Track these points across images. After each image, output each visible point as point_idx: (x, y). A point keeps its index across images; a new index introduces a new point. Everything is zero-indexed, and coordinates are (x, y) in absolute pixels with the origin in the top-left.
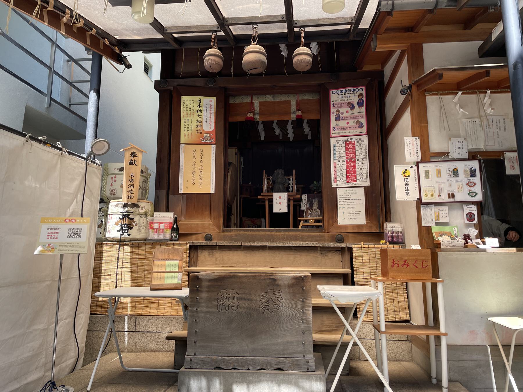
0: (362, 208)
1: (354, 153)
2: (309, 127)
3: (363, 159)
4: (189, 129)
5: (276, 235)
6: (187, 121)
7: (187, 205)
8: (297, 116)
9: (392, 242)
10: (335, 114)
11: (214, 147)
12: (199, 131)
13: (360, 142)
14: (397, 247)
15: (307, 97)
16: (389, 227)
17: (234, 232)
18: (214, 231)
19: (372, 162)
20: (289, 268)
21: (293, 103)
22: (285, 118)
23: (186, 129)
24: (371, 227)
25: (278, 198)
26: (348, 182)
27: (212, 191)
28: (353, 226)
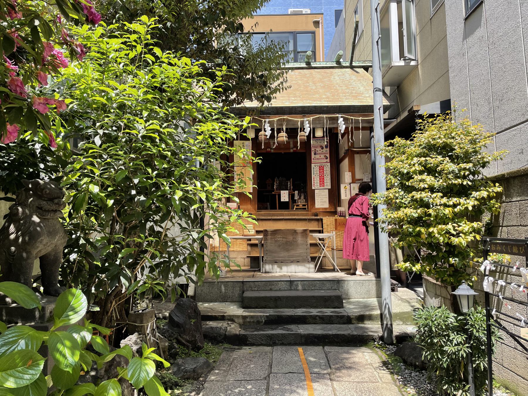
0: (327, 200)
9: (340, 216)
14: (342, 218)
16: (339, 209)
17: (263, 212)
20: (300, 227)
28: (323, 208)
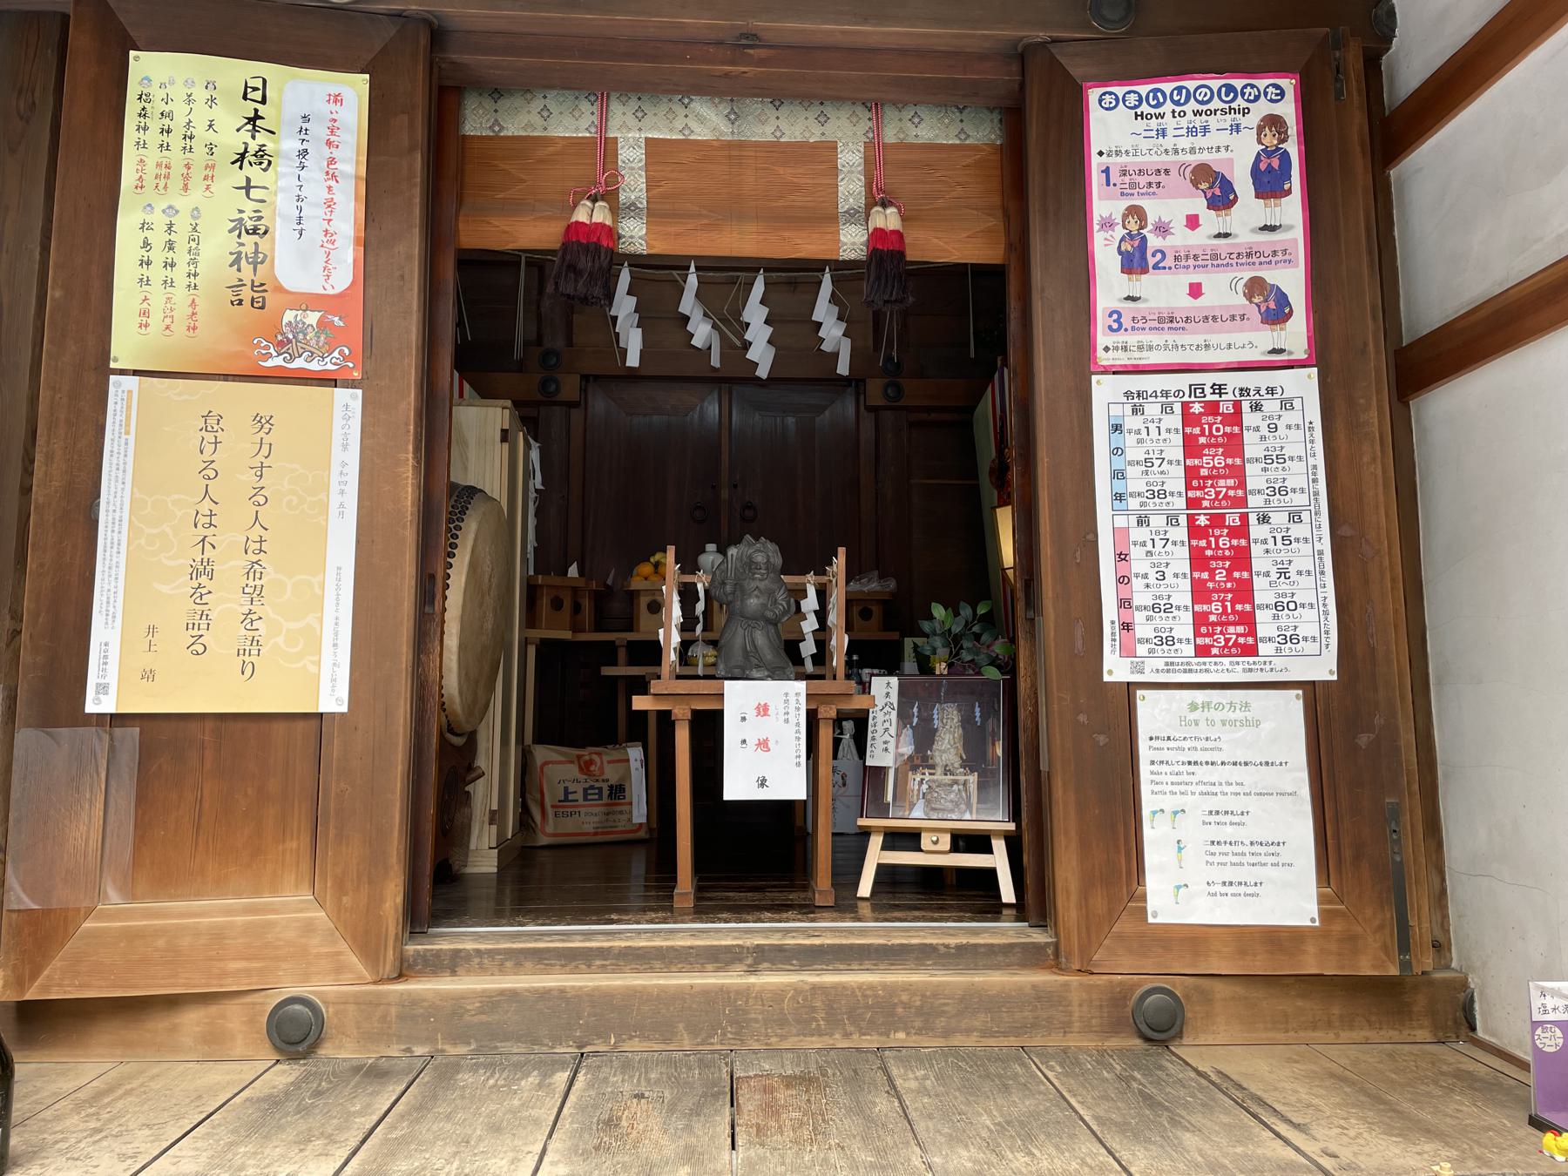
1: (1239, 474)
2: (840, 318)
3: (1295, 517)
4: (179, 275)
5: (760, 995)
6: (159, 219)
7: (143, 798)
8: (878, 235)
10: (1119, 232)
11: (349, 402)
12: (246, 294)
13: (1271, 406)
15: (928, 129)
18: (332, 979)
19: (1345, 531)
21: (851, 158)
22: (806, 246)
23: (157, 273)
24: (1351, 942)
25: (751, 714)
26: (1202, 651)
27: (333, 698)
